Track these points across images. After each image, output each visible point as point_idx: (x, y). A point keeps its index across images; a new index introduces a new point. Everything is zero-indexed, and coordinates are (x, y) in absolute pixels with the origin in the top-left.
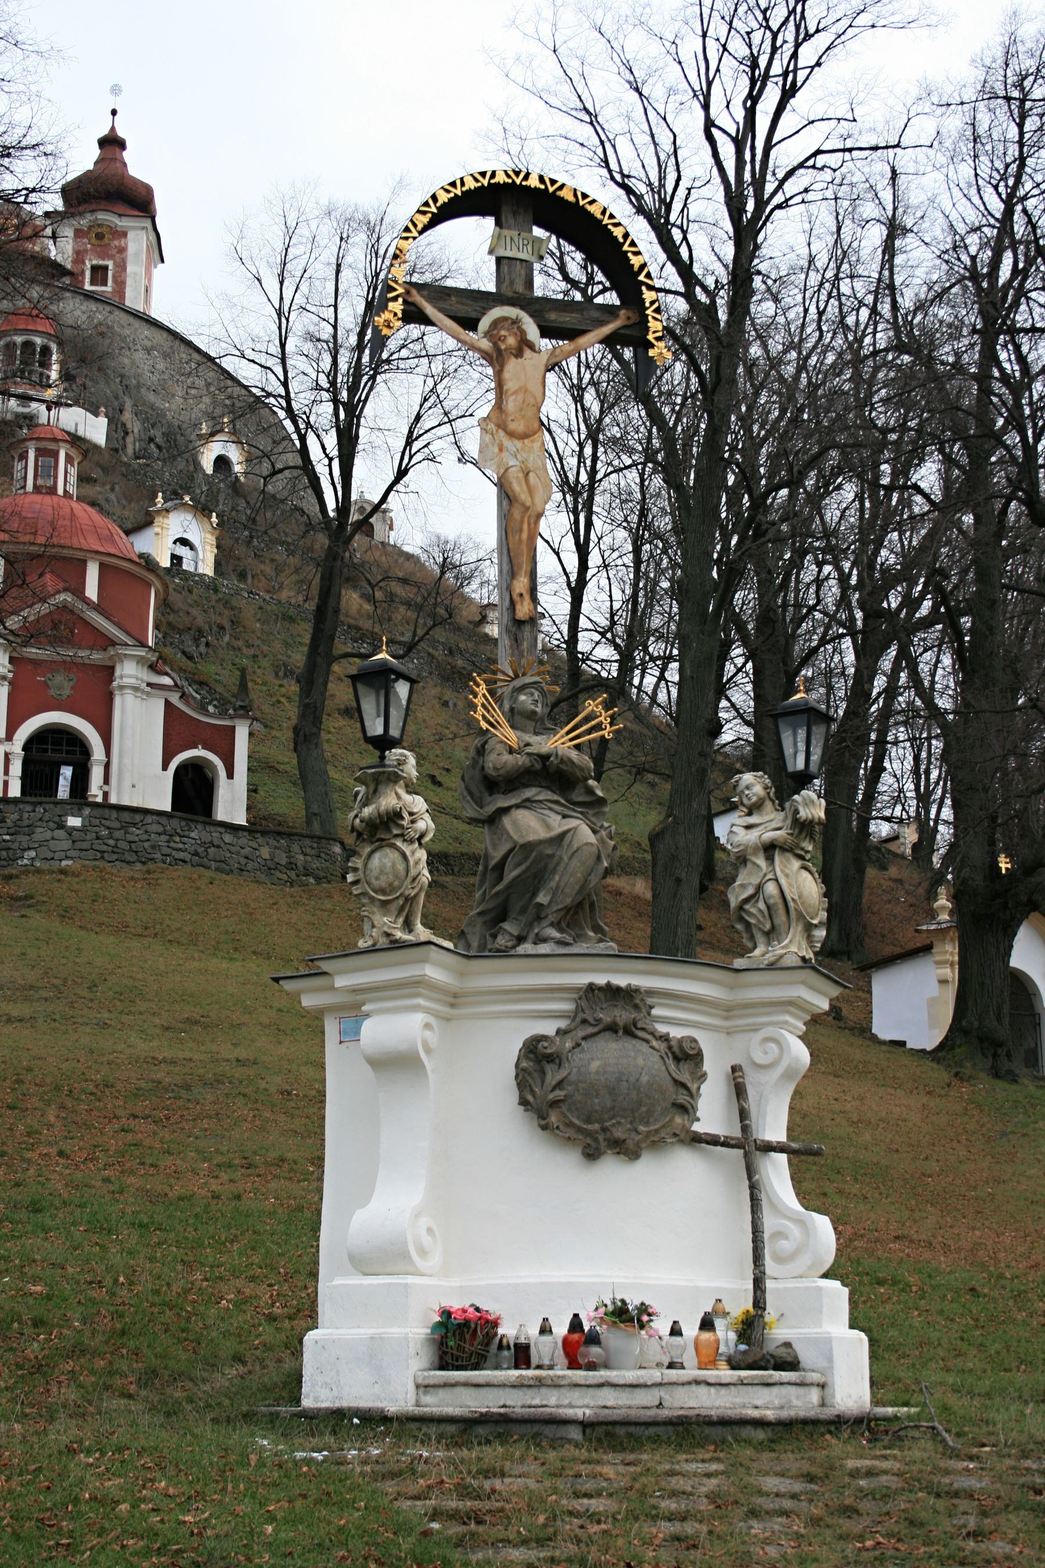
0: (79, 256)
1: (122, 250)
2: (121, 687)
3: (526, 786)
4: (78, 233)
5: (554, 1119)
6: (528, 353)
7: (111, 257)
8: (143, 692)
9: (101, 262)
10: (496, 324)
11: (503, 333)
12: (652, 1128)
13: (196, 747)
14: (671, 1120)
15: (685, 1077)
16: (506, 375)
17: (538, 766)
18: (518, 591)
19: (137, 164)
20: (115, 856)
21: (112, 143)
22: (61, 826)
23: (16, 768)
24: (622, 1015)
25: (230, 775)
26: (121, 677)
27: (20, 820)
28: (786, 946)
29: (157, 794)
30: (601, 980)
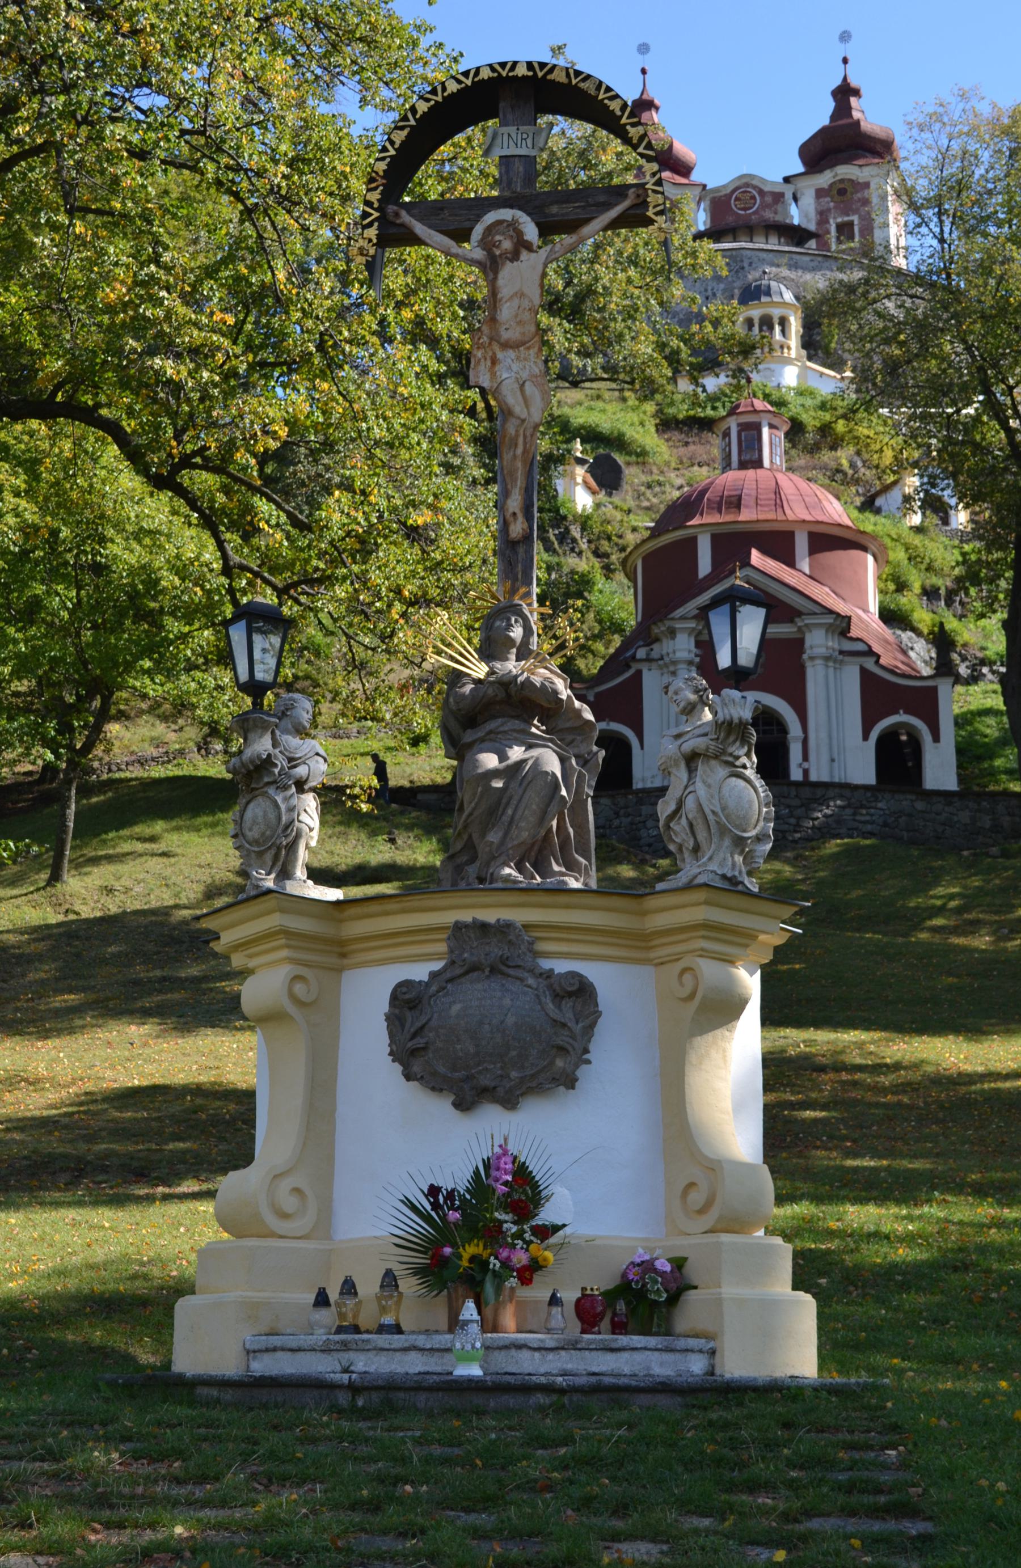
0: (823, 217)
1: (866, 202)
3: (494, 717)
4: (820, 193)
5: (416, 1069)
6: (524, 255)
7: (856, 212)
9: (846, 219)
10: (489, 230)
11: (498, 238)
12: (529, 1072)
13: (897, 712)
14: (552, 1063)
15: (567, 1015)
16: (500, 282)
17: (501, 695)
18: (511, 510)
19: (871, 114)
21: (844, 93)
24: (496, 950)
25: (936, 738)
26: (811, 647)
28: (705, 864)
29: (861, 767)
30: (466, 916)
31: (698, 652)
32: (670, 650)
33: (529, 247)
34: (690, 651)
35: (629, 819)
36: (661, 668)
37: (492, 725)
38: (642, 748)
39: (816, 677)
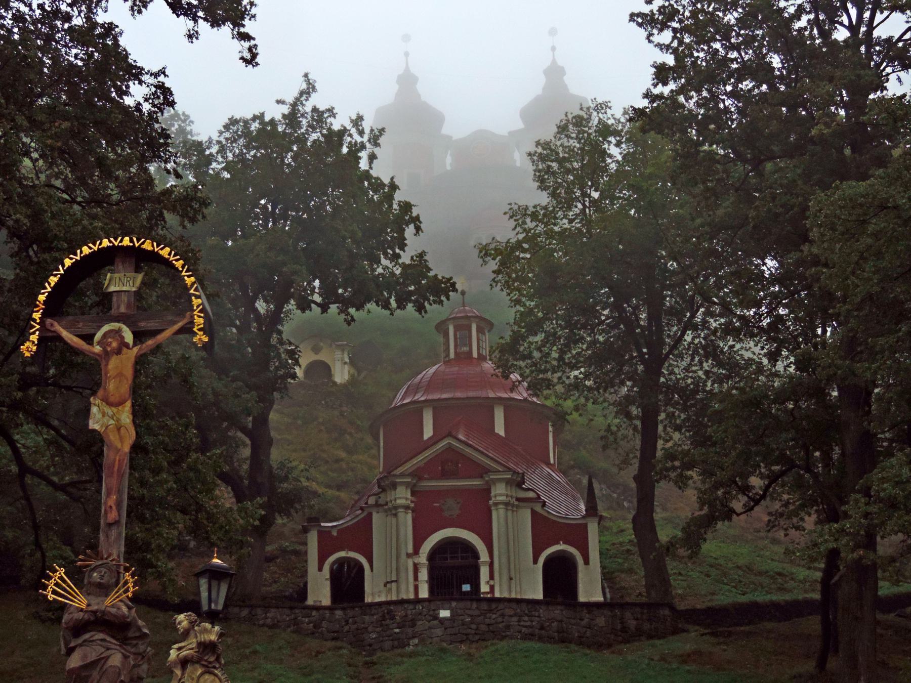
2: (496, 504)
3: (85, 633)
6: (125, 350)
8: (513, 505)
10: (105, 336)
11: (110, 340)
13: (558, 543)
20: (477, 637)
22: (436, 617)
23: (424, 575)
26: (495, 496)
27: (406, 616)
31: (413, 499)
32: (393, 498)
33: (127, 345)
34: (407, 499)
35: (355, 626)
36: (386, 511)
37: (87, 636)
38: (372, 570)
39: (498, 517)
